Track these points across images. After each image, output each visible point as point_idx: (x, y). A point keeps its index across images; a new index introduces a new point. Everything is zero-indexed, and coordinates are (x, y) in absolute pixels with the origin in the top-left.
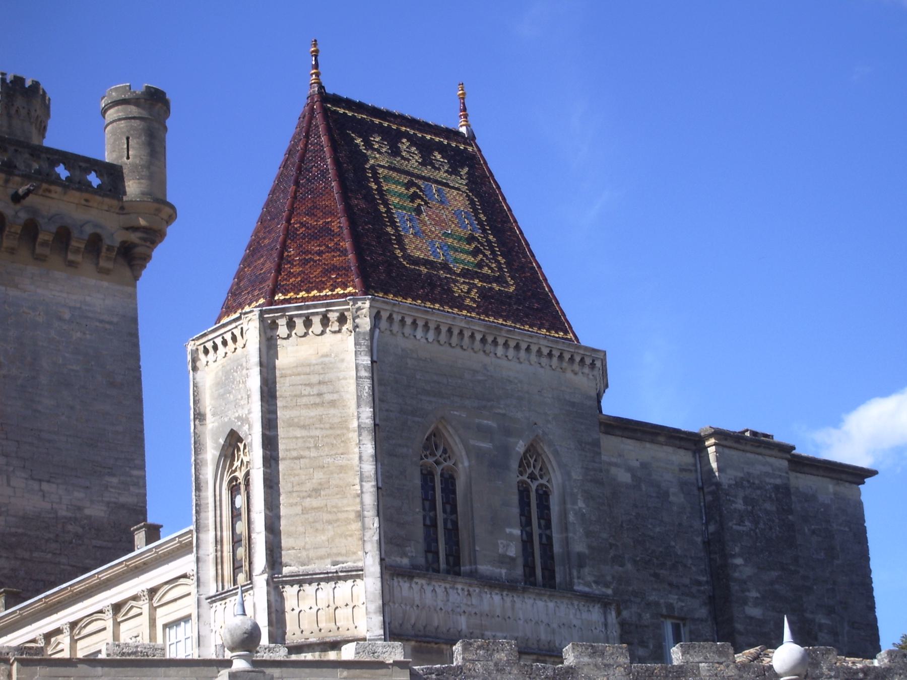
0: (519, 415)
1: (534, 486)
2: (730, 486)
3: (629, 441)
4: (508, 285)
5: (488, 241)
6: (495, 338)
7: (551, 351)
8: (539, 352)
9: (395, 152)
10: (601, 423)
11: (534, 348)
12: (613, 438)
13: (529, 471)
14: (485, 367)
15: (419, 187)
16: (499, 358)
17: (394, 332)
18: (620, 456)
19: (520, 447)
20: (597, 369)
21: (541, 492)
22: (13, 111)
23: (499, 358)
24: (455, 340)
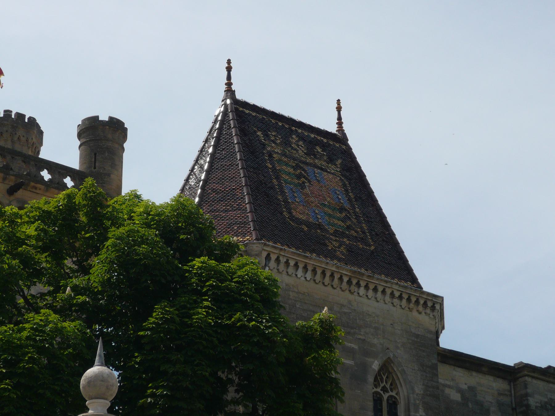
0: (375, 341)
1: (385, 396)
2: (536, 407)
3: (459, 369)
4: (370, 246)
5: (355, 213)
6: (359, 281)
7: (401, 294)
8: (392, 294)
9: (286, 143)
10: (439, 354)
11: (388, 291)
12: (447, 366)
13: (382, 385)
14: (350, 302)
15: (304, 170)
16: (361, 297)
17: (281, 270)
18: (453, 380)
19: (376, 365)
20: (436, 311)
21: (390, 402)
22: (16, 138)
23: (361, 297)
24: (327, 280)
